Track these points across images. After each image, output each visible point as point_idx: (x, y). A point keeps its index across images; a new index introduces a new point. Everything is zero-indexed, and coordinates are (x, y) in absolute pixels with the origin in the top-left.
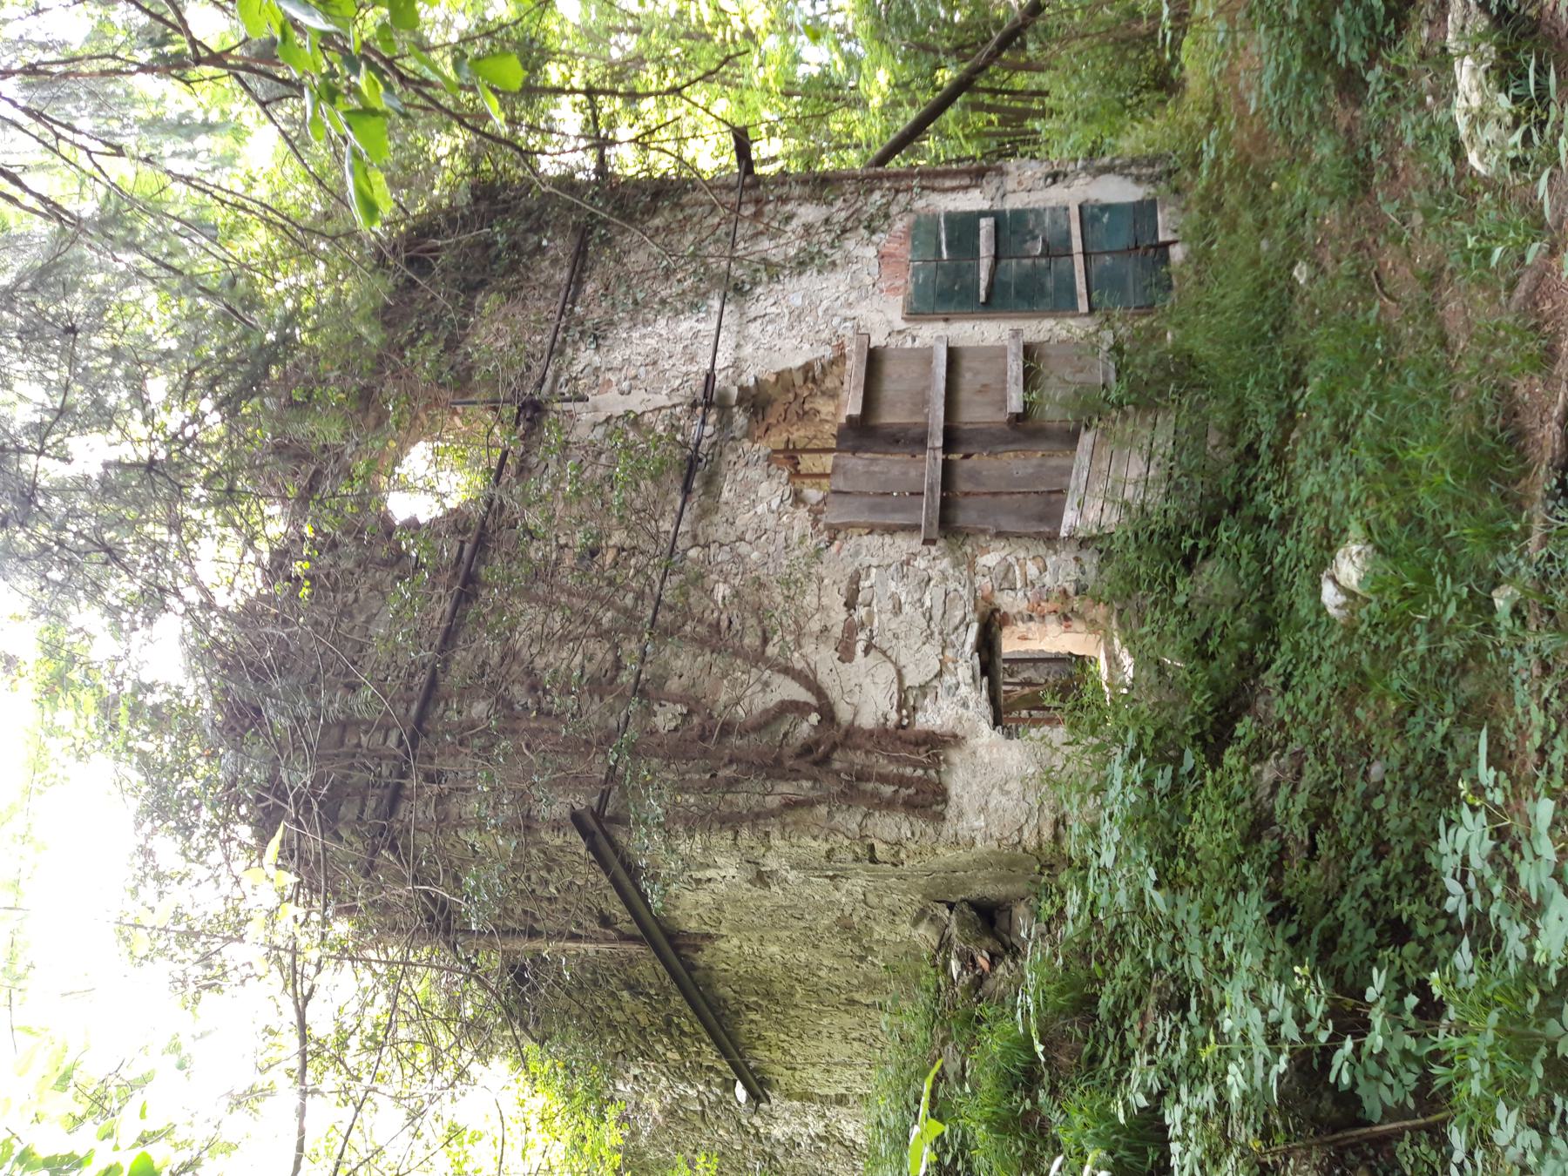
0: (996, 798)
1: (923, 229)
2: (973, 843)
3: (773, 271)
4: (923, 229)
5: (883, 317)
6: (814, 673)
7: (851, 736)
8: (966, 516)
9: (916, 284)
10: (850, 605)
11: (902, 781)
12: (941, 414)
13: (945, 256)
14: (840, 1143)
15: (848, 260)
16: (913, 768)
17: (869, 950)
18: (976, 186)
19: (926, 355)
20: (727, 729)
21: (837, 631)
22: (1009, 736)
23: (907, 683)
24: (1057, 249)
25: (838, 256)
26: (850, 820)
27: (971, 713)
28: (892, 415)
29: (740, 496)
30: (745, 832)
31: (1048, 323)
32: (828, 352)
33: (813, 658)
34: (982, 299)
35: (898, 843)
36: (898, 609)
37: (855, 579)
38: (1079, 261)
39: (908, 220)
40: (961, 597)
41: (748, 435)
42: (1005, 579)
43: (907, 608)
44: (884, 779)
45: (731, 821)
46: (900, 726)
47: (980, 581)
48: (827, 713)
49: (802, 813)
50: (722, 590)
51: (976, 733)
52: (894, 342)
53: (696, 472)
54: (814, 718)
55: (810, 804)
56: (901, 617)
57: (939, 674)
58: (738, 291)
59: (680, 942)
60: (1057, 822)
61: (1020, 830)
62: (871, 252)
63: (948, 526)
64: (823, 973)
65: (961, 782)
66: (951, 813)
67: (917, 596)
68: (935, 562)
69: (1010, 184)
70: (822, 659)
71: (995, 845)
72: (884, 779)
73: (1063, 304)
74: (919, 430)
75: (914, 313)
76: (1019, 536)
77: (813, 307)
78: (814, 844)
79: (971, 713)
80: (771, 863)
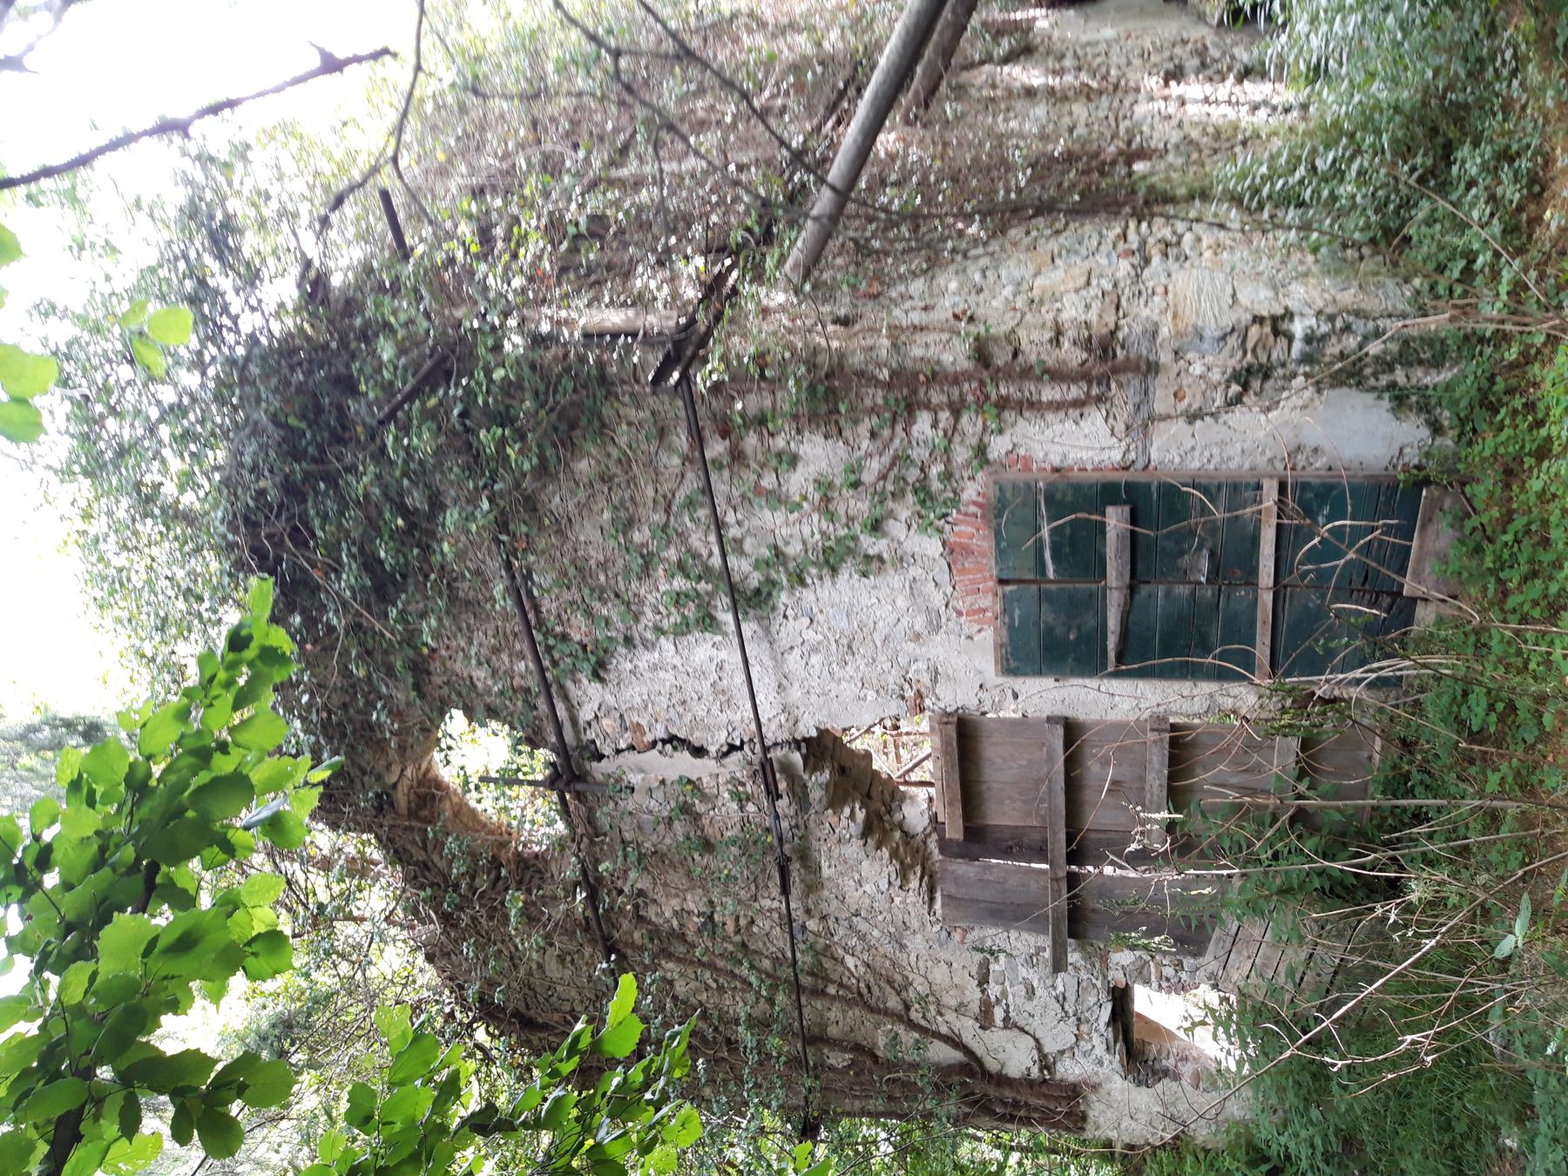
0: (1126, 1122)
1: (1013, 507)
4: (1013, 507)
6: (959, 1036)
9: (1011, 627)
10: (983, 981)
13: (1051, 574)
18: (1100, 400)
21: (975, 1007)
22: (1139, 1084)
24: (1234, 562)
28: (1002, 813)
36: (1031, 992)
40: (1094, 986)
43: (1039, 992)
47: (1111, 975)
56: (1035, 1002)
58: (753, 601)
67: (1049, 982)
70: (968, 1029)
74: (1036, 836)
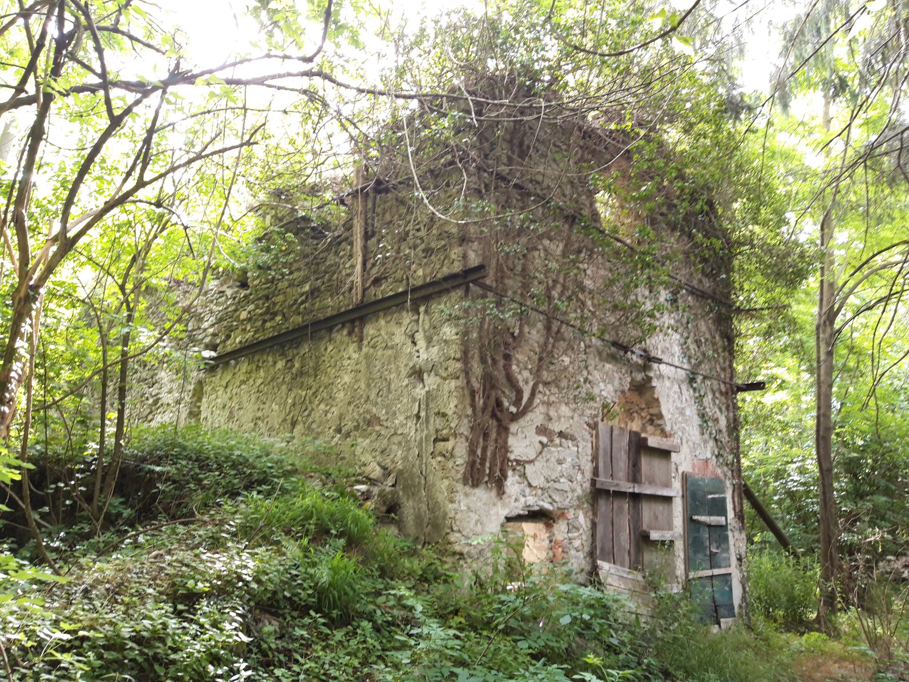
0: (474, 517)
2: (452, 502)
3: (700, 399)
5: (684, 461)
7: (504, 430)
8: (603, 504)
10: (561, 434)
11: (483, 460)
12: (648, 492)
14: (150, 413)
15: (705, 442)
16: (488, 468)
17: (348, 435)
19: (667, 485)
20: (507, 357)
23: (527, 466)
24: (713, 560)
25: (706, 436)
26: (464, 429)
27: (513, 503)
28: (645, 463)
29: (607, 373)
30: (459, 365)
31: (682, 555)
32: (668, 429)
33: (537, 410)
34: (695, 517)
35: (452, 456)
36: (560, 462)
37: (573, 438)
38: (709, 573)
39: (721, 476)
41: (632, 380)
42: (572, 527)
43: (559, 468)
44: (484, 449)
45: (465, 358)
46: (509, 460)
48: (515, 418)
49: (468, 401)
50: (567, 360)
51: (504, 506)
52: (673, 466)
53: (617, 350)
54: (513, 409)
55: (473, 405)
57: (530, 485)
59: (357, 323)
60: (461, 554)
61: (459, 531)
62: (709, 455)
63: (598, 494)
64: (322, 406)
65: (482, 495)
66: (467, 489)
68: (581, 485)
69: (737, 534)
70: (536, 417)
71: (452, 515)
72: (484, 449)
73: (689, 564)
75: (685, 478)
76: (593, 536)
77: (686, 421)
78: (452, 405)
79: (513, 503)
80: (431, 381)
